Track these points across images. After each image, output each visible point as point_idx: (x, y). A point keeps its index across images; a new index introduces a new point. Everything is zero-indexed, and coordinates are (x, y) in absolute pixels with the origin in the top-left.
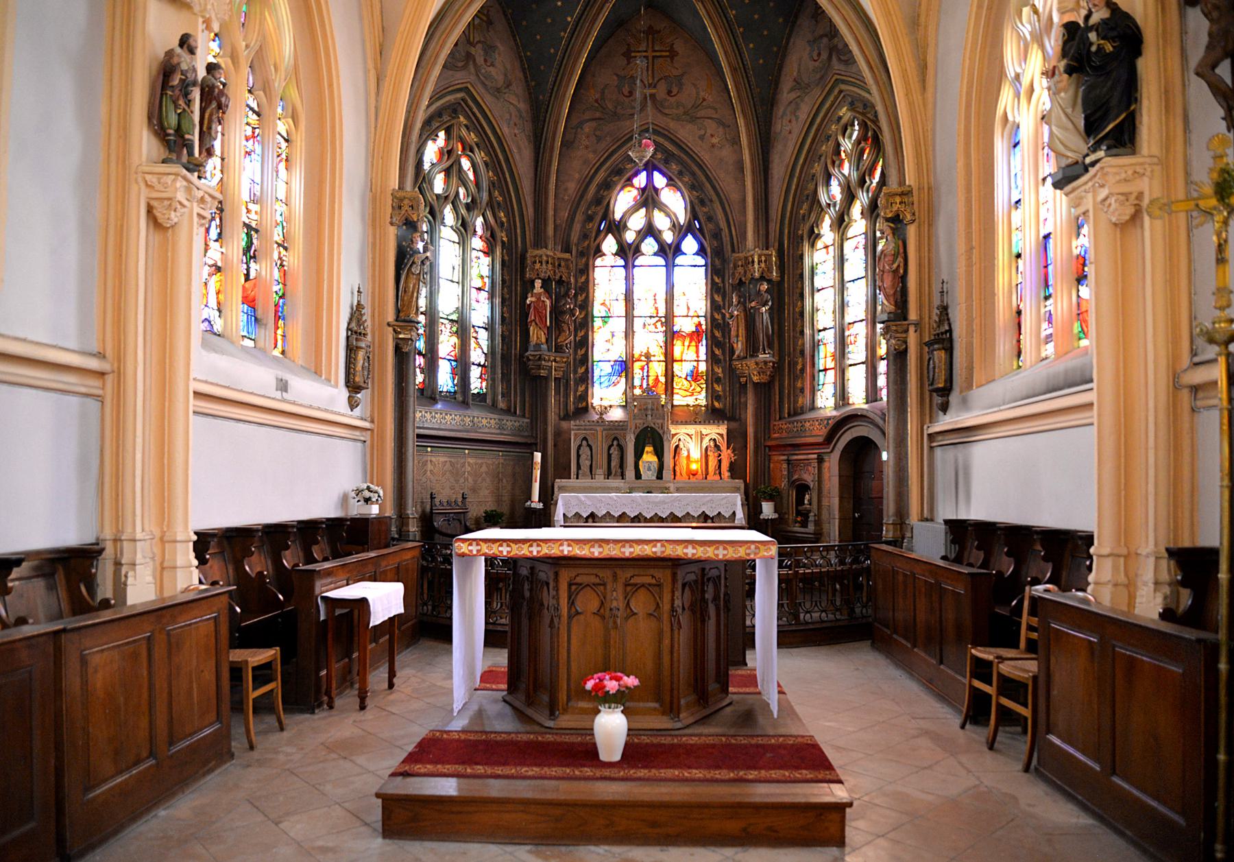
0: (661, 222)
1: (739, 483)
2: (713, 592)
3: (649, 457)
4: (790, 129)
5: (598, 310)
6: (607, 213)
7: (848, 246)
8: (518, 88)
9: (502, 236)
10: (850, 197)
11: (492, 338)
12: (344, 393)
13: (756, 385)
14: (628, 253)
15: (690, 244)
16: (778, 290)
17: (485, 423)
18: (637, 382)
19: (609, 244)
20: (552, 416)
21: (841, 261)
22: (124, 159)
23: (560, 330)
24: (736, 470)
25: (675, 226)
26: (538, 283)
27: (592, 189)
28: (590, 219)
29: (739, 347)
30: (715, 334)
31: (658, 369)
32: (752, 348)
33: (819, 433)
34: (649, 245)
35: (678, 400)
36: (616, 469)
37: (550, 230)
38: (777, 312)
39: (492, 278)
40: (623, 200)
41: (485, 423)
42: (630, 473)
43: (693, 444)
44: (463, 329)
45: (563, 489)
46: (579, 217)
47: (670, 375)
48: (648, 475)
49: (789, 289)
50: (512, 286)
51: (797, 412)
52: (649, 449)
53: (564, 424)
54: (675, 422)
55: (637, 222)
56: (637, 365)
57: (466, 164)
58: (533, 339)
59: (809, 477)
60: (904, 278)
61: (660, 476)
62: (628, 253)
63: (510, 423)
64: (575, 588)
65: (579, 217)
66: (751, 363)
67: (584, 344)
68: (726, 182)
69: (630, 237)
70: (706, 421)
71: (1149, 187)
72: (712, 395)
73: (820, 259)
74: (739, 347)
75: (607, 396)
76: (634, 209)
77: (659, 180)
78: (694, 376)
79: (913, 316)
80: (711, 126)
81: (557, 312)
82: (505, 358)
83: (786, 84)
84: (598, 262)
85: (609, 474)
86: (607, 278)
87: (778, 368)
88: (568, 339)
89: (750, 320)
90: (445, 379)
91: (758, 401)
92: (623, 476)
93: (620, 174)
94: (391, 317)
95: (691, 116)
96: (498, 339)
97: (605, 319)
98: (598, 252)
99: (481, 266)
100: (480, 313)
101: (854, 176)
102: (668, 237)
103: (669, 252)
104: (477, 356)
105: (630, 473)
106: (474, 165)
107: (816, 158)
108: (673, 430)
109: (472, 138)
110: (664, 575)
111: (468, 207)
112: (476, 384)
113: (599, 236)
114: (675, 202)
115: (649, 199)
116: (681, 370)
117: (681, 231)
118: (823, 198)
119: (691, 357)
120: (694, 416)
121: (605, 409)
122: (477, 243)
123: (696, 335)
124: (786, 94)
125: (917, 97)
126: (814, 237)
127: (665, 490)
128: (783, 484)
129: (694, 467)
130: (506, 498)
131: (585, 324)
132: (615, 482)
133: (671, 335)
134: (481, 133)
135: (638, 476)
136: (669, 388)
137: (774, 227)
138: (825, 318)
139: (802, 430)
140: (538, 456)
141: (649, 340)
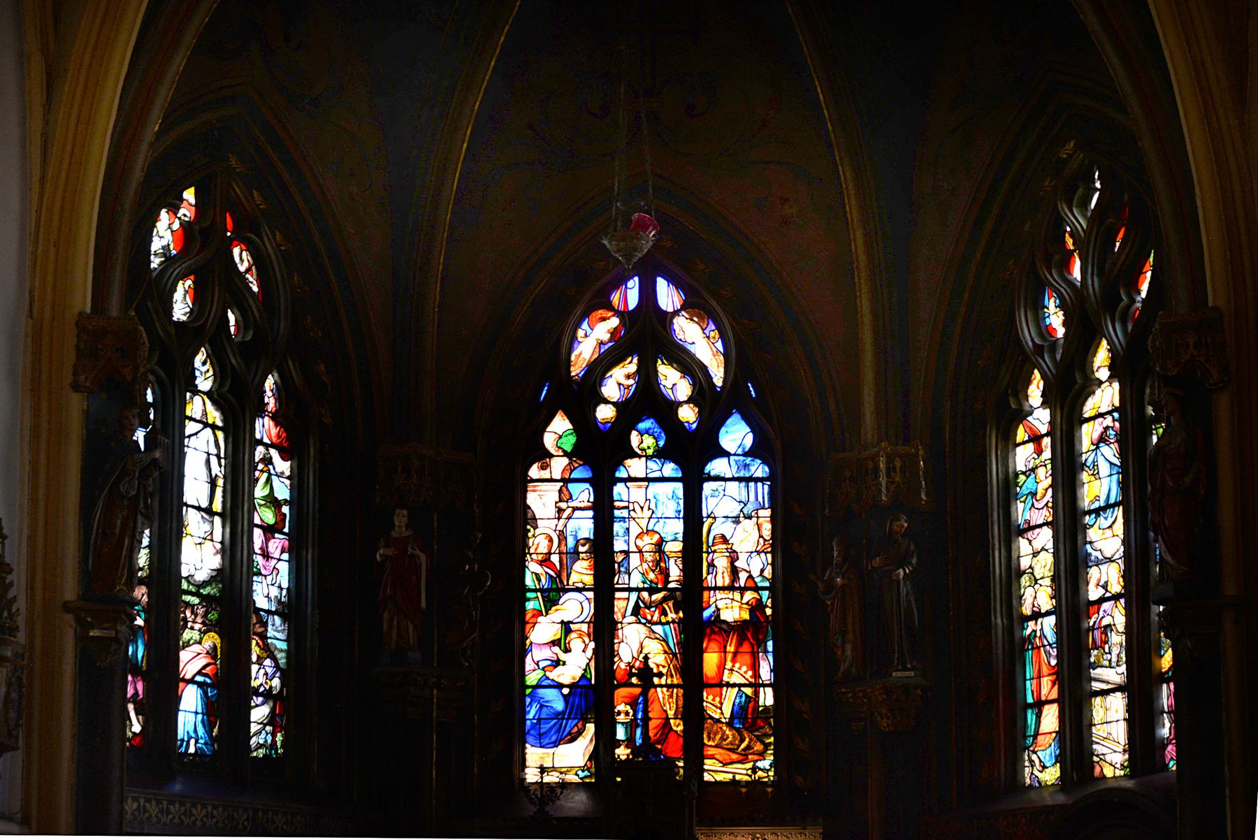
0: (674, 383)
14: (601, 455)
21: (1068, 470)
26: (400, 518)
47: (693, 713)
62: (601, 455)
77: (667, 296)
94: (70, 591)
103: (691, 454)
115: (647, 337)
116: (721, 706)
119: (740, 679)
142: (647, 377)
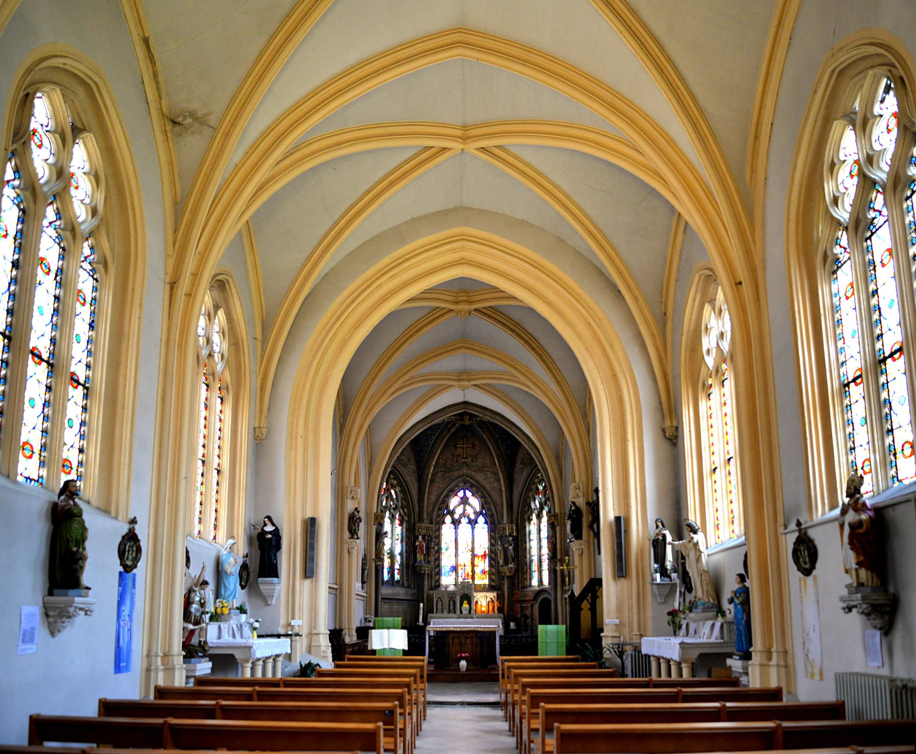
0: (469, 511)
1: (501, 615)
2: (486, 637)
3: (466, 605)
4: (520, 478)
5: (443, 546)
6: (447, 507)
7: (542, 525)
8: (412, 461)
9: (406, 518)
10: (542, 508)
11: (402, 558)
12: (360, 584)
13: (508, 577)
14: (456, 523)
15: (481, 519)
16: (516, 539)
17: (400, 592)
18: (460, 575)
19: (448, 519)
20: (426, 589)
21: (539, 530)
22: (342, 538)
23: (429, 556)
24: (500, 610)
25: (475, 512)
26: (420, 537)
27: (442, 497)
28: (440, 509)
29: (501, 562)
30: (492, 556)
31: (469, 569)
32: (506, 562)
33: (530, 596)
34: (464, 521)
35: (477, 582)
36: (452, 610)
37: (425, 516)
38: (516, 549)
39: (402, 534)
40: (454, 502)
41: (400, 592)
42: (458, 612)
43: (483, 600)
44: (392, 556)
45: (431, 618)
46: (436, 509)
47: (473, 572)
48: (465, 612)
49: (520, 540)
50: (410, 539)
51: (524, 587)
52: (465, 602)
53: (431, 592)
54: (476, 591)
55: (459, 511)
56: (460, 568)
57: (393, 492)
58: (419, 559)
59: (528, 613)
60: (555, 544)
61: (470, 612)
62: (456, 523)
63: (410, 592)
64: (453, 638)
65: (436, 509)
66: (506, 568)
67: (438, 559)
68: (495, 495)
69: (456, 516)
70: (488, 591)
71: (585, 547)
72: (491, 580)
73: (532, 527)
74: (501, 562)
75: (448, 581)
76: (459, 505)
77: (469, 494)
78: (484, 572)
79: (559, 557)
80: (489, 475)
81: (428, 548)
82: (407, 565)
83: (519, 461)
84: (444, 526)
85: (449, 612)
86: (447, 530)
87: (517, 570)
88: (432, 559)
89: (505, 551)
90: (386, 577)
91: (509, 584)
92: (455, 612)
93: (453, 492)
94: (374, 557)
95: (481, 469)
96: (404, 559)
97: (447, 549)
98: (444, 523)
99: (398, 530)
100: (398, 549)
101: (543, 500)
102: (472, 517)
103: (473, 523)
104: (397, 566)
105: (458, 612)
106: (396, 493)
107: (529, 491)
108: (475, 594)
109: (395, 482)
110: (473, 635)
111: (394, 509)
112: (397, 577)
113: (444, 516)
114: (475, 502)
115: (464, 501)
116: (478, 570)
117: (478, 514)
118: (533, 506)
119: (483, 565)
120: (483, 589)
121: (447, 587)
122: (397, 522)
123: (484, 556)
124: (519, 466)
125: (559, 482)
126: (530, 520)
127: (472, 618)
128: (519, 615)
129: (484, 609)
130: (408, 621)
131: (439, 551)
132: (451, 615)
133: (474, 556)
134: (399, 480)
135: (461, 612)
136: (473, 578)
137: (515, 515)
138: (534, 551)
139: (525, 596)
140: (421, 605)
141: (465, 558)
142: (465, 510)
